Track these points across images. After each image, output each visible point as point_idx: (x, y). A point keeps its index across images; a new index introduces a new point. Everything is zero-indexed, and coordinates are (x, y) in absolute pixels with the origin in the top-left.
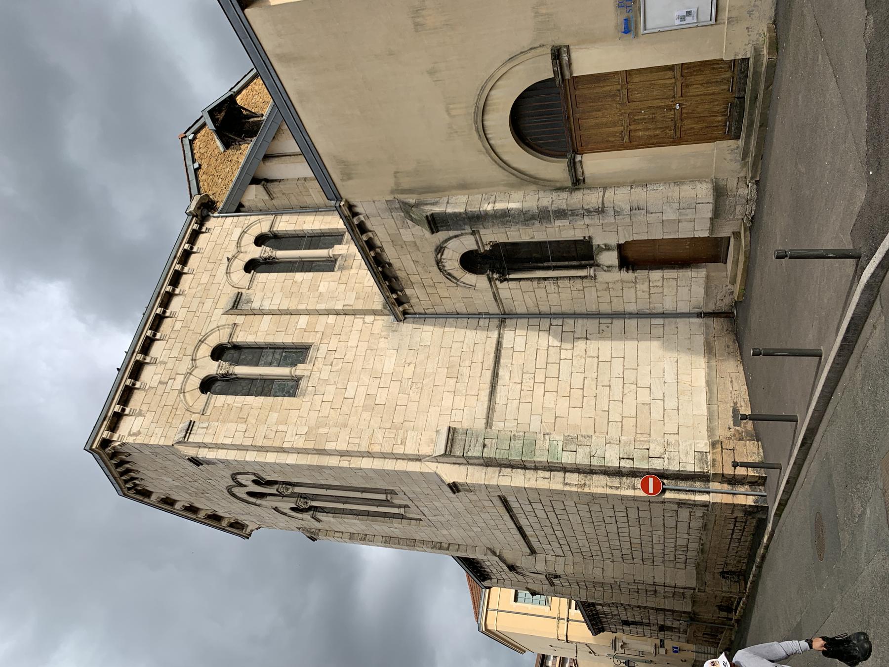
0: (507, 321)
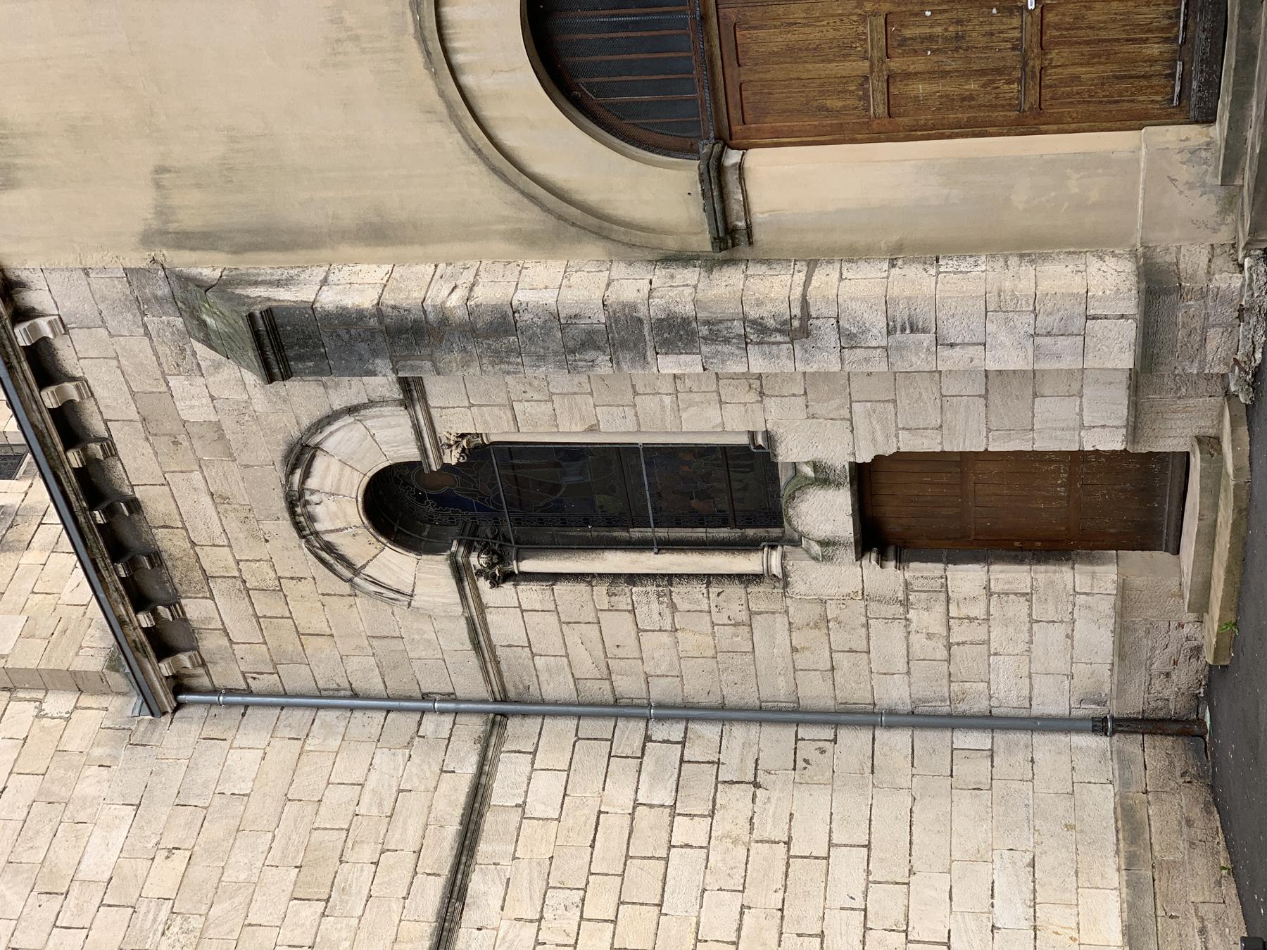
0: (513, 724)
